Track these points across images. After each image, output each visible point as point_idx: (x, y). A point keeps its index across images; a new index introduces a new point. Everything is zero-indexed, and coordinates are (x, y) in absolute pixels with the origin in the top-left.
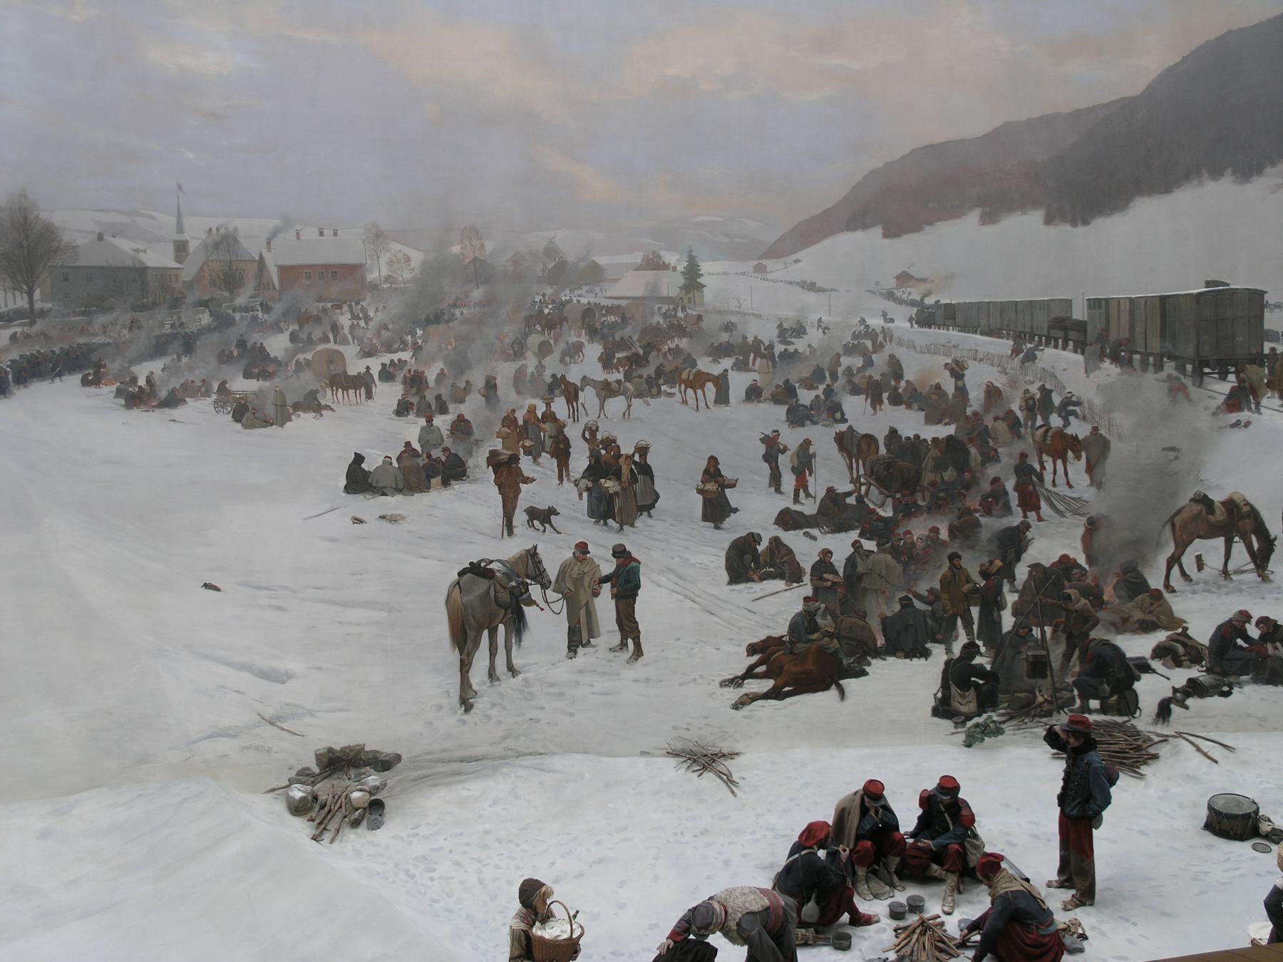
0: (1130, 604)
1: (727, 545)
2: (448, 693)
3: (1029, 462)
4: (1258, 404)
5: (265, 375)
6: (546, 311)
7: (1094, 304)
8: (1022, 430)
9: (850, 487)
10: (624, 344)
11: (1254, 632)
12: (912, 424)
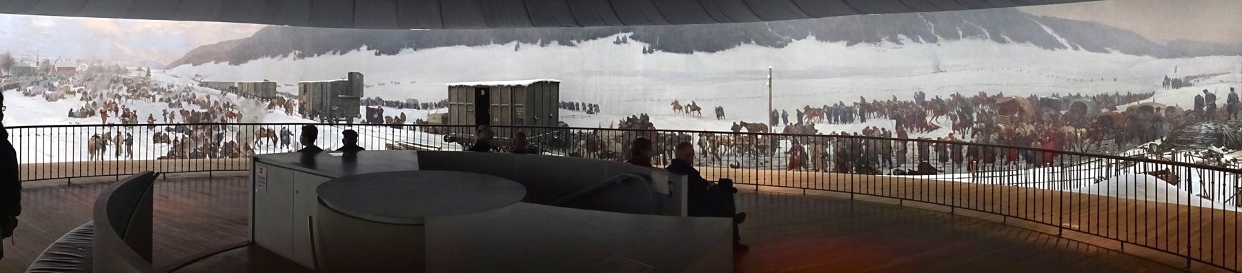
5: (53, 90)
7: (240, 83)
10: (132, 87)
12: (198, 109)
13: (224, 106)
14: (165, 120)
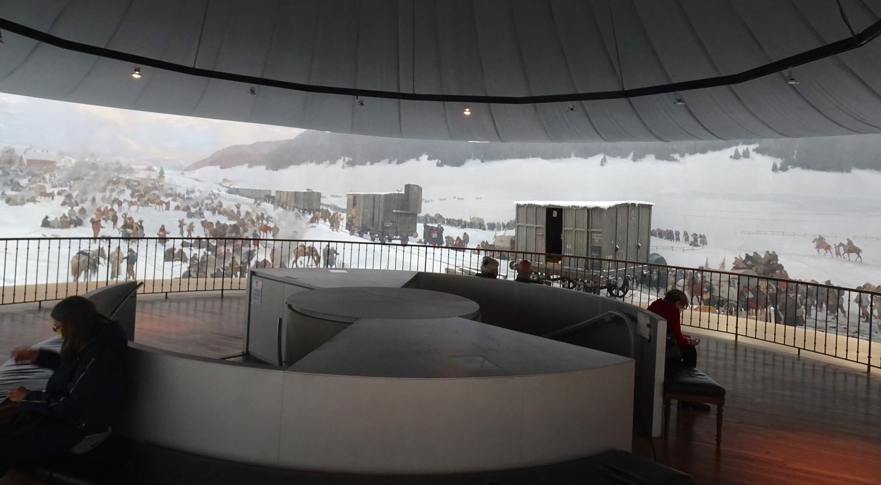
5: (18, 190)
6: (114, 180)
8: (255, 224)
10: (138, 191)
12: (224, 220)
13: (258, 218)
14: (182, 232)
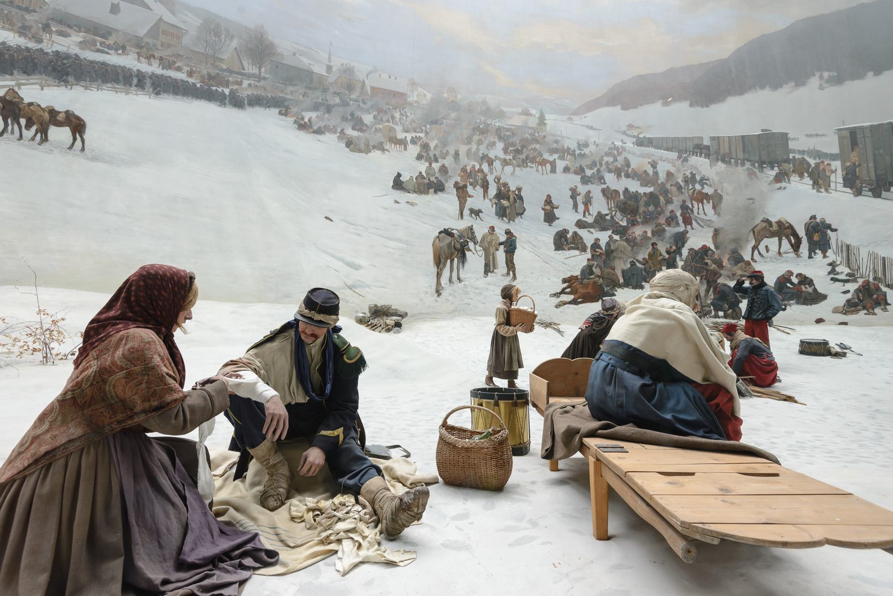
0: (736, 267)
1: (554, 233)
2: (430, 286)
3: (687, 204)
4: (789, 180)
6: (481, 127)
8: (683, 190)
9: (608, 212)
10: (513, 144)
11: (795, 280)
12: (634, 186)
13: (686, 181)
